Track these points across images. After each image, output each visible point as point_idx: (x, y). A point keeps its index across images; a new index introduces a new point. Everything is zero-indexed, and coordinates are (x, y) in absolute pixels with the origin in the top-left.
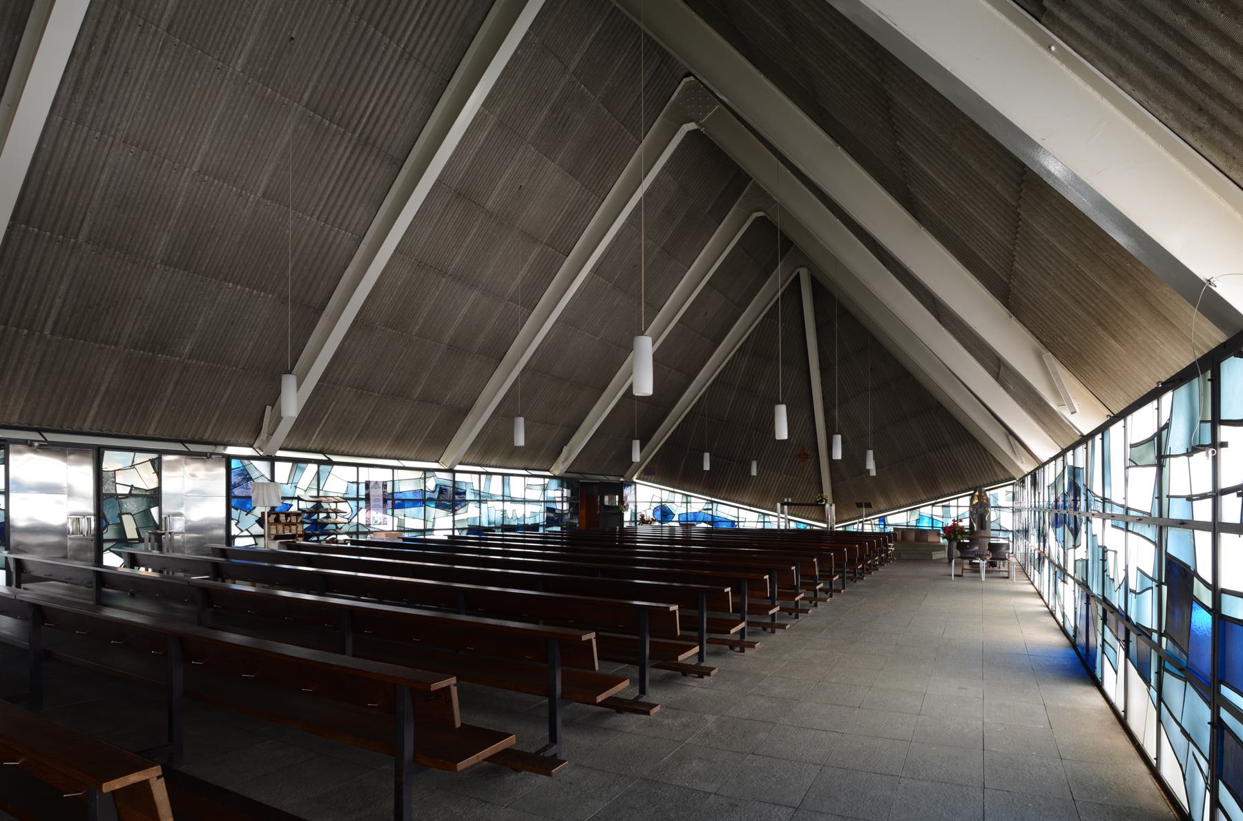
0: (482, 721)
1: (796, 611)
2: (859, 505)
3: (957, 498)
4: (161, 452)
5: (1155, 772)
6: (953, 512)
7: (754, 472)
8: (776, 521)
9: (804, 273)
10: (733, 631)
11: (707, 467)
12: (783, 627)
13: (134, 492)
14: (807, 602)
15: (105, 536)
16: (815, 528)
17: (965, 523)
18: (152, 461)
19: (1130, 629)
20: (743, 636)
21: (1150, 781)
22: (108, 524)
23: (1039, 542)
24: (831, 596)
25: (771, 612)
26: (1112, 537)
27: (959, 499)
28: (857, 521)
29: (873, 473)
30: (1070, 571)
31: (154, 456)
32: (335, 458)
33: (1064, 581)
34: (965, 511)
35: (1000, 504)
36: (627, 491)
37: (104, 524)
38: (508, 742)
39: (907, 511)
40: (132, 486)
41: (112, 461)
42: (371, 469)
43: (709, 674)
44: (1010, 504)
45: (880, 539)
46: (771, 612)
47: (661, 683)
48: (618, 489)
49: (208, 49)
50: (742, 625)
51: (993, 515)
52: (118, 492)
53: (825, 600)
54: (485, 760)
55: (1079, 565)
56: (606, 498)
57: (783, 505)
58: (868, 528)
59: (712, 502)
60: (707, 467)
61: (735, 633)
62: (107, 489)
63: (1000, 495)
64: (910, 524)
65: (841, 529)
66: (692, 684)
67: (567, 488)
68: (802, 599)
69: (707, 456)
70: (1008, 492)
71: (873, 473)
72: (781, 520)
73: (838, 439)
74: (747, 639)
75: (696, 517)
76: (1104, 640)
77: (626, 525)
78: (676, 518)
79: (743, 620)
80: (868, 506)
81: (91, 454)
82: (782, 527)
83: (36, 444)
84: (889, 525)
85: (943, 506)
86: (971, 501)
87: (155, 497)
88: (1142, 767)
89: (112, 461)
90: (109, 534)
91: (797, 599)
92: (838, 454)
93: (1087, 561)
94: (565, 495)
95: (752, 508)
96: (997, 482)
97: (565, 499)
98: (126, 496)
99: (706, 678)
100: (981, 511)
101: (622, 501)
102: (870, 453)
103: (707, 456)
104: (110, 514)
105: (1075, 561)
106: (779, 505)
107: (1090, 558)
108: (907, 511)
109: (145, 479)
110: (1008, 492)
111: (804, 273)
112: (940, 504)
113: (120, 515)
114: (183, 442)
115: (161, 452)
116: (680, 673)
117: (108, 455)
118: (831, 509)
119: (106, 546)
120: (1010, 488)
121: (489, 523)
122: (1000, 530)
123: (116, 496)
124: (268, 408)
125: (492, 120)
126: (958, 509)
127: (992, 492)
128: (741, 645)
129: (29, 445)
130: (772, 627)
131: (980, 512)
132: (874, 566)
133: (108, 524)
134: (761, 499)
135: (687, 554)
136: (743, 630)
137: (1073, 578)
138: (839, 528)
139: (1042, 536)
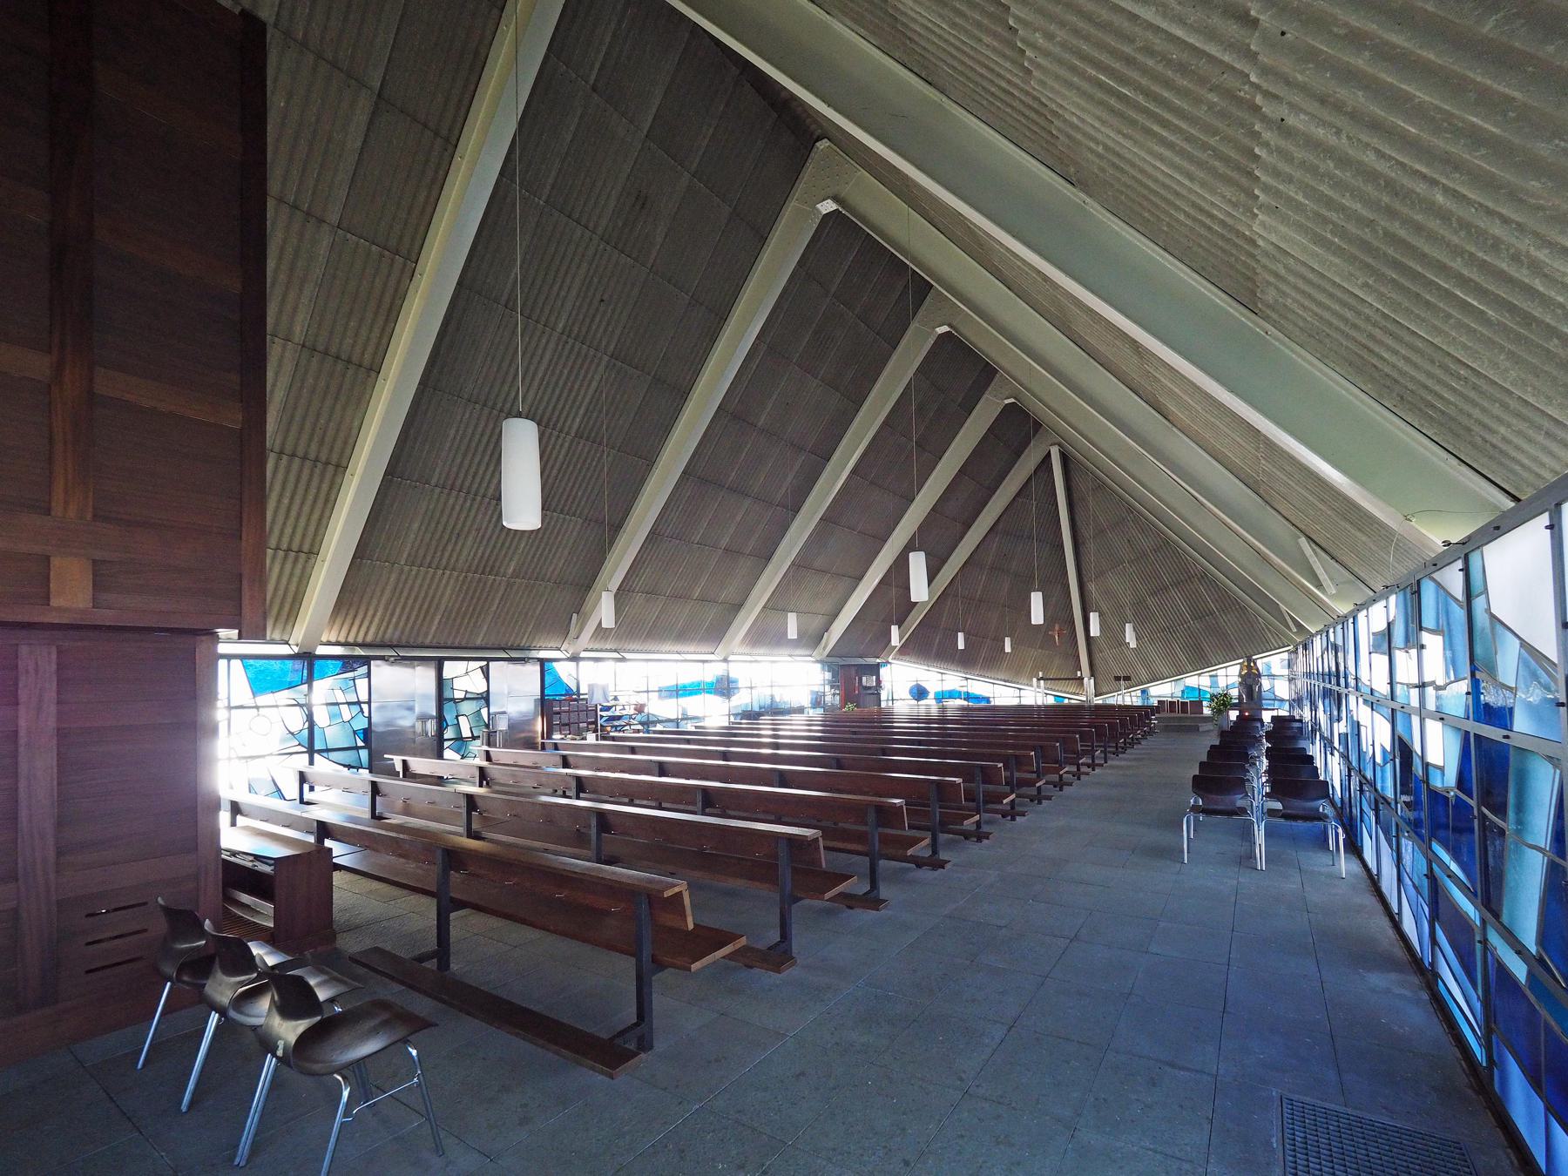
0: (714, 921)
1: (1060, 785)
2: (1118, 679)
3: (1226, 667)
4: (489, 660)
5: (1396, 925)
6: (1222, 683)
7: (1008, 649)
8: (1034, 695)
9: (1055, 451)
10: (1005, 802)
11: (961, 646)
12: (1049, 798)
13: (468, 696)
14: (1071, 776)
15: (446, 737)
16: (1073, 701)
17: (1234, 693)
18: (481, 668)
19: (1379, 802)
20: (1013, 808)
21: (1391, 932)
22: (447, 725)
23: (1311, 711)
24: (1093, 770)
25: (1038, 785)
26: (1363, 714)
27: (1228, 668)
28: (1116, 694)
29: (1133, 645)
30: (1336, 744)
31: (484, 663)
32: (627, 656)
33: (1332, 754)
34: (1236, 680)
35: (1273, 673)
36: (882, 671)
37: (445, 725)
38: (743, 941)
39: (1171, 681)
40: (466, 692)
41: (450, 669)
42: (650, 663)
43: (988, 838)
44: (1286, 672)
45: (1139, 716)
46: (1038, 785)
47: (950, 845)
48: (875, 670)
49: (528, 311)
50: (1013, 796)
51: (1266, 684)
52: (455, 697)
53: (1087, 774)
54: (724, 957)
55: (1342, 738)
56: (864, 679)
57: (1039, 680)
58: (1128, 701)
59: (967, 679)
60: (961, 646)
61: (1006, 804)
62: (447, 694)
63: (1273, 663)
64: (1174, 695)
65: (1100, 702)
66: (974, 847)
67: (829, 671)
68: (1066, 773)
69: (961, 636)
70: (1283, 660)
71: (1133, 645)
72: (1038, 694)
73: (1094, 618)
74: (1018, 809)
75: (952, 695)
76: (1361, 809)
77: (883, 705)
78: (931, 695)
79: (1012, 792)
80: (1127, 678)
81: (434, 665)
82: (1040, 703)
83: (392, 659)
84: (1152, 697)
85: (1211, 676)
86: (1241, 669)
87: (485, 698)
88: (1385, 923)
89: (450, 669)
90: (449, 734)
91: (1061, 772)
92: (1095, 631)
93: (1347, 734)
94: (827, 678)
95: (1008, 684)
96: (1267, 647)
97: (826, 682)
98: (463, 700)
99: (985, 841)
100: (1249, 681)
101: (879, 681)
102: (1129, 628)
103: (961, 636)
104: (449, 717)
105: (1339, 734)
106: (1035, 680)
107: (1349, 732)
108: (1171, 681)
109: (477, 684)
110: (1283, 660)
111: (1055, 451)
112: (1207, 674)
113: (457, 717)
114: (504, 649)
115: (489, 660)
116: (963, 838)
117: (447, 664)
118: (1089, 683)
119: (446, 744)
120: (1285, 656)
121: (760, 708)
122: (1274, 700)
123: (453, 700)
124: (575, 615)
125: (764, 347)
126: (1228, 677)
127: (1265, 660)
128: (1012, 813)
129: (382, 658)
130: (1039, 798)
131: (1250, 680)
132: (1137, 739)
133: (447, 725)
134: (1015, 672)
135: (944, 733)
136: (1013, 801)
137: (1338, 751)
138: (1098, 701)
139: (1314, 707)
